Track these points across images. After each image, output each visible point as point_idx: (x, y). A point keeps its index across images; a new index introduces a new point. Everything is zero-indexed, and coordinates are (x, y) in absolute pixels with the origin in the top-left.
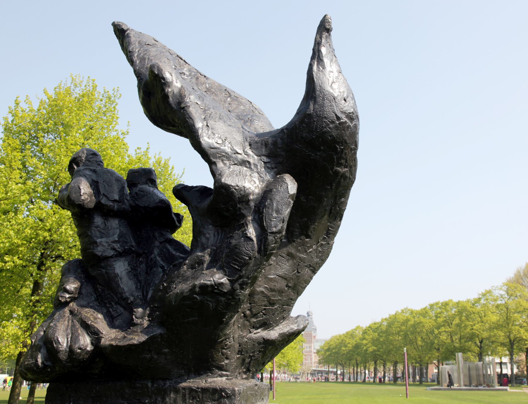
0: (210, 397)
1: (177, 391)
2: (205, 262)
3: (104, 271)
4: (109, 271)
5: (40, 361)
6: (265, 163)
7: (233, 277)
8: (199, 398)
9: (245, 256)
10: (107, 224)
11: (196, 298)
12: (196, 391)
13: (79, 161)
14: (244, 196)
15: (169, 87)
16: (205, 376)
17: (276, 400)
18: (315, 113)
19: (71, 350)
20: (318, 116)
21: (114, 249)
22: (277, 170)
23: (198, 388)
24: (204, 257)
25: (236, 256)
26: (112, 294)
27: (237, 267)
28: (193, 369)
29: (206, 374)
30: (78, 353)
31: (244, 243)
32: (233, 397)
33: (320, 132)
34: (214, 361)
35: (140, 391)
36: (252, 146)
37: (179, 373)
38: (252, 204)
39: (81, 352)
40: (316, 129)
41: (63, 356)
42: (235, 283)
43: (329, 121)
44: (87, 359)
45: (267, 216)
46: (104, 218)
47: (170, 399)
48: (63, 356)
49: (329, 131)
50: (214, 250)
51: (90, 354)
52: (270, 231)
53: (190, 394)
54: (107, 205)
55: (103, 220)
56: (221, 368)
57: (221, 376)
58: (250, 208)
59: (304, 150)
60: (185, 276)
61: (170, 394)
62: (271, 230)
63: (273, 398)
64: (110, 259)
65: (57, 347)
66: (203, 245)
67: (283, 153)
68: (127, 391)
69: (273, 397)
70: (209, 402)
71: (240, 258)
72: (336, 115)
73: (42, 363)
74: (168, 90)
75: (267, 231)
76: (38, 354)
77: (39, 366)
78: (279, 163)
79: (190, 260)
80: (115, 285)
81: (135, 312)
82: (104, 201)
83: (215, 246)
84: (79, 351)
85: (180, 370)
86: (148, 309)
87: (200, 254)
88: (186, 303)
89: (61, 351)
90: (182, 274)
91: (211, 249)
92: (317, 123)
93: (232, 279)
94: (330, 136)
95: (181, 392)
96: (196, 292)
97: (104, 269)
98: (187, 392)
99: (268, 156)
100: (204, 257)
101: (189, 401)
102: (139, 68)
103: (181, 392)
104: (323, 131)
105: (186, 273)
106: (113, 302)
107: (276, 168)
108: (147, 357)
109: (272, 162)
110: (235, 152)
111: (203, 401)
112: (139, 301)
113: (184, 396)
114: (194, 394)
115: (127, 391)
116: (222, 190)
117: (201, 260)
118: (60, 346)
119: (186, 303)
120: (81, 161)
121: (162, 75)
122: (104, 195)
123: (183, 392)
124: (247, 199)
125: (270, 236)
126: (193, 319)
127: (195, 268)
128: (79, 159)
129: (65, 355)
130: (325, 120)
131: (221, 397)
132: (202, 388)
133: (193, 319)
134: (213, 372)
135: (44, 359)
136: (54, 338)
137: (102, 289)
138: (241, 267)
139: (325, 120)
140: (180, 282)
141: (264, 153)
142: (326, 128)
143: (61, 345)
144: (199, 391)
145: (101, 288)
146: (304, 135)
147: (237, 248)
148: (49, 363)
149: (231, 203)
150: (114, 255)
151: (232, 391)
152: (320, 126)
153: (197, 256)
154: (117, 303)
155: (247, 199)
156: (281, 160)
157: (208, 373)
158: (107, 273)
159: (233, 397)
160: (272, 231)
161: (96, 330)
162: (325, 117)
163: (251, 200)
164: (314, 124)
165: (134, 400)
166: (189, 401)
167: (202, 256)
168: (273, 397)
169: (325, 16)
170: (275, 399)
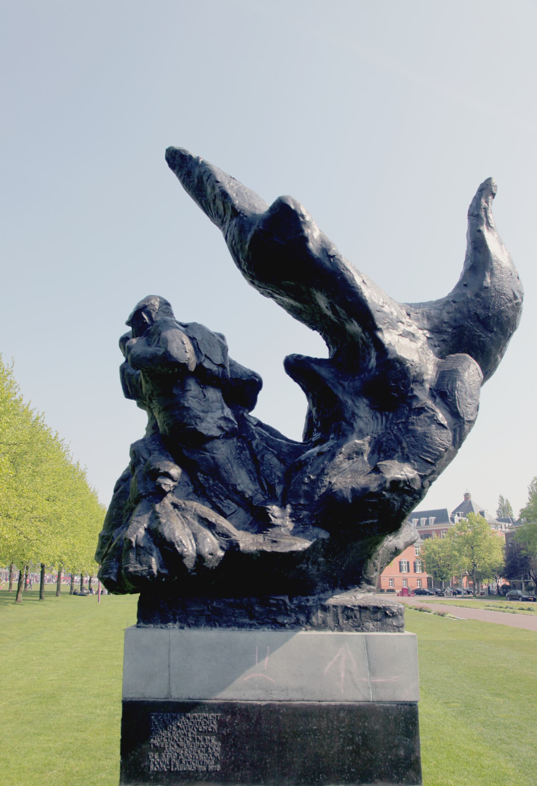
0: (370, 617)
1: (325, 609)
2: (365, 451)
3: (208, 454)
4: (215, 455)
5: (155, 568)
6: (428, 338)
7: (423, 471)
8: (355, 617)
9: (439, 447)
10: (206, 395)
11: (384, 495)
12: (352, 610)
13: (151, 311)
14: (419, 374)
15: (309, 227)
16: (353, 590)
17: (101, 603)
18: (493, 287)
19: (200, 558)
20: (497, 292)
21: (220, 428)
22: (440, 349)
23: (354, 606)
24: (364, 445)
25: (428, 446)
26: (221, 485)
27: (429, 459)
28: (340, 582)
29: (354, 588)
30: (209, 559)
31: (436, 431)
32: (400, 617)
33: (497, 309)
34: (365, 573)
35: (274, 609)
36: (411, 316)
37: (324, 588)
38: (427, 386)
39: (212, 558)
40: (494, 306)
41: (189, 563)
42: (425, 479)
43: (507, 299)
44: (216, 567)
45: (460, 400)
46: (202, 386)
47: (317, 619)
48: (189, 563)
49: (506, 311)
50: (375, 438)
51: (221, 561)
52: (467, 420)
53: (343, 612)
54: (210, 370)
55: (201, 389)
56: (369, 582)
57: (369, 591)
58: (425, 389)
59: (475, 329)
60: (341, 468)
61: (317, 611)
62: (468, 418)
63: (98, 602)
64: (216, 440)
65: (182, 551)
66: (361, 431)
67: (450, 330)
68: (257, 609)
69: (98, 600)
70: (369, 622)
71: (433, 449)
72: (514, 293)
73: (158, 571)
74: (308, 232)
75: (463, 419)
76: (151, 559)
77: (154, 575)
78: (444, 341)
79: (347, 448)
80: (225, 474)
81: (269, 509)
82: (207, 364)
83: (375, 433)
84: (210, 557)
85: (325, 584)
86: (288, 506)
87: (357, 441)
88: (371, 501)
89: (187, 555)
90: (338, 465)
91: (372, 437)
92: (495, 299)
93: (423, 474)
94: (506, 317)
95: (332, 611)
96: (385, 487)
97: (208, 452)
98: (340, 611)
99: (431, 331)
100: (364, 445)
101: (343, 622)
102: (239, 202)
103: (332, 611)
104: (501, 310)
105: (342, 464)
106: (222, 495)
107: (439, 346)
108: (303, 567)
109: (435, 339)
110: (398, 320)
111: (361, 620)
112: (261, 496)
113: (336, 615)
114: (350, 613)
115: (257, 609)
116: (396, 363)
117: (360, 449)
118: (185, 550)
119: (371, 501)
120: (154, 310)
121: (301, 212)
122: (206, 356)
123: (334, 611)
124: (422, 378)
125: (467, 425)
126: (372, 521)
127: (353, 459)
128: (152, 308)
129: (191, 562)
130: (503, 297)
131: (386, 615)
132: (360, 607)
133: (372, 521)
134: (362, 586)
135: (159, 566)
136: (175, 539)
137: (205, 479)
138: (435, 460)
139: (503, 297)
140: (335, 475)
141: (426, 327)
142: (504, 306)
143: (185, 547)
144: (357, 610)
145: (203, 477)
146: (479, 310)
147: (427, 437)
148: (164, 571)
149: (403, 381)
150: (221, 435)
151: (398, 609)
152: (498, 303)
153: (355, 444)
154: (227, 497)
155: (422, 378)
156: (446, 337)
157: (356, 587)
158: (213, 458)
159: (400, 617)
160: (469, 419)
161: (225, 530)
162: (504, 294)
163: (427, 380)
164: (492, 299)
165: (266, 620)
166: (343, 622)
167: (361, 445)
168: (98, 600)
169: (489, 179)
170: (100, 603)
